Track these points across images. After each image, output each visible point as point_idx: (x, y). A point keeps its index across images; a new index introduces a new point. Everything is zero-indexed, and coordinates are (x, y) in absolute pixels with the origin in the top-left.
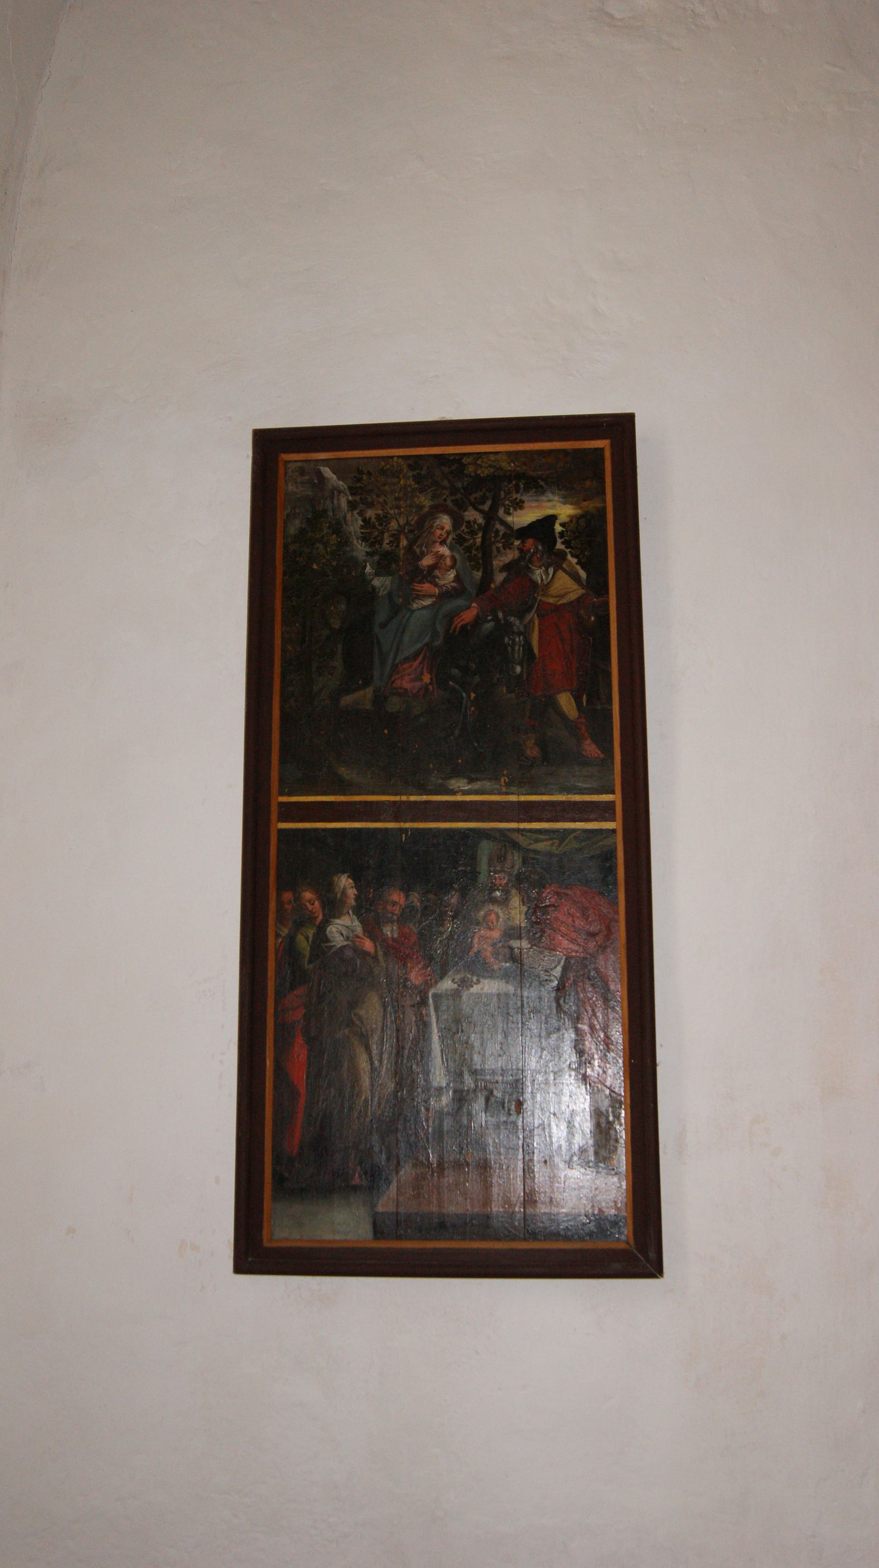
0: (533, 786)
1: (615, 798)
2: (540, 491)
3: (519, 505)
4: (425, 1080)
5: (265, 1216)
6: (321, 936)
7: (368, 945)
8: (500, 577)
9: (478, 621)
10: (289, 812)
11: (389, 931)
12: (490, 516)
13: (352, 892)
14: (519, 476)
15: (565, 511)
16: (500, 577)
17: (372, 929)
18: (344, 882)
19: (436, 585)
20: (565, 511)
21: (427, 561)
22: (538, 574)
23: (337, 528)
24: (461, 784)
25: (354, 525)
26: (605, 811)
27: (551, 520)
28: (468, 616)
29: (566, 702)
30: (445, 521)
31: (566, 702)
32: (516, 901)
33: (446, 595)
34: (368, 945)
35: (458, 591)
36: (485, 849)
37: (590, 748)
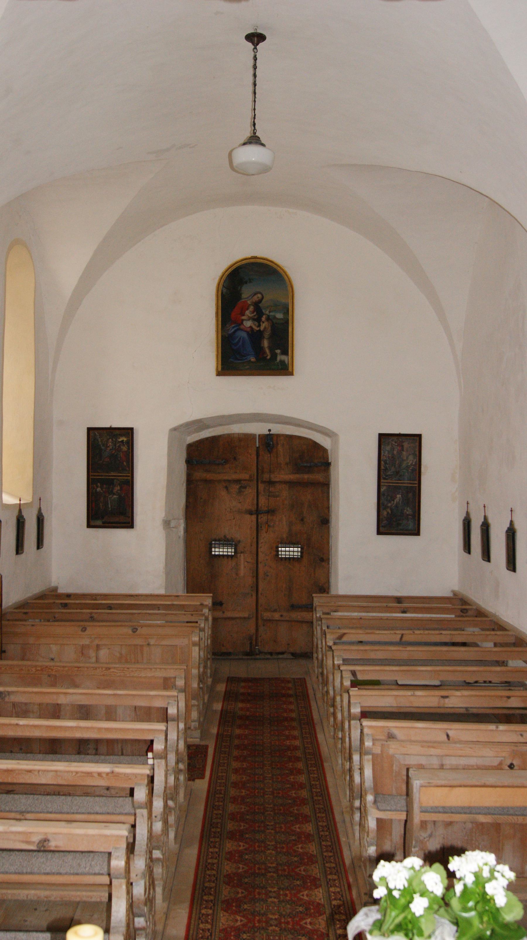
0: (121, 473)
1: (130, 475)
2: (122, 436)
3: (120, 438)
4: (178, 779)
5: (331, 791)
6: (96, 490)
7: (102, 491)
8: (117, 447)
9: (115, 453)
10: (92, 476)
11: (104, 490)
12: (116, 439)
13: (100, 485)
14: (120, 435)
15: (125, 439)
16: (117, 447)
17: (102, 489)
18: (99, 484)
19: (114, 494)
20: (125, 439)
21: (108, 445)
22: (122, 447)
23: (98, 440)
24: (112, 473)
25: (100, 440)
26: (129, 476)
27: (123, 440)
28: (113, 452)
29: (125, 463)
30: (111, 440)
31: (125, 463)
32: (118, 486)
33: (111, 449)
34: (102, 491)
35: (112, 449)
36: (115, 481)
37: (127, 469)
